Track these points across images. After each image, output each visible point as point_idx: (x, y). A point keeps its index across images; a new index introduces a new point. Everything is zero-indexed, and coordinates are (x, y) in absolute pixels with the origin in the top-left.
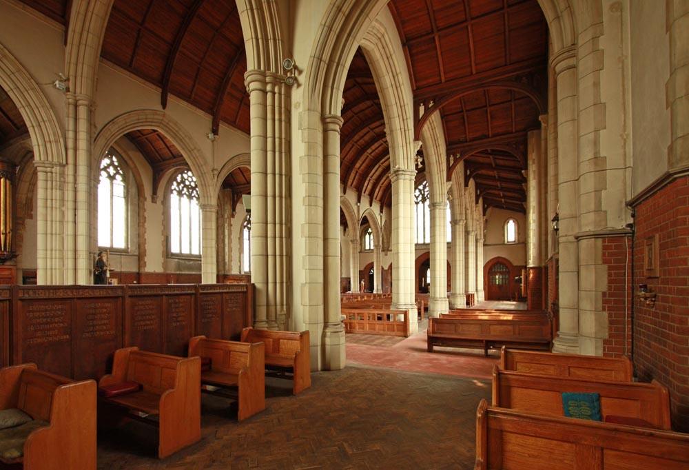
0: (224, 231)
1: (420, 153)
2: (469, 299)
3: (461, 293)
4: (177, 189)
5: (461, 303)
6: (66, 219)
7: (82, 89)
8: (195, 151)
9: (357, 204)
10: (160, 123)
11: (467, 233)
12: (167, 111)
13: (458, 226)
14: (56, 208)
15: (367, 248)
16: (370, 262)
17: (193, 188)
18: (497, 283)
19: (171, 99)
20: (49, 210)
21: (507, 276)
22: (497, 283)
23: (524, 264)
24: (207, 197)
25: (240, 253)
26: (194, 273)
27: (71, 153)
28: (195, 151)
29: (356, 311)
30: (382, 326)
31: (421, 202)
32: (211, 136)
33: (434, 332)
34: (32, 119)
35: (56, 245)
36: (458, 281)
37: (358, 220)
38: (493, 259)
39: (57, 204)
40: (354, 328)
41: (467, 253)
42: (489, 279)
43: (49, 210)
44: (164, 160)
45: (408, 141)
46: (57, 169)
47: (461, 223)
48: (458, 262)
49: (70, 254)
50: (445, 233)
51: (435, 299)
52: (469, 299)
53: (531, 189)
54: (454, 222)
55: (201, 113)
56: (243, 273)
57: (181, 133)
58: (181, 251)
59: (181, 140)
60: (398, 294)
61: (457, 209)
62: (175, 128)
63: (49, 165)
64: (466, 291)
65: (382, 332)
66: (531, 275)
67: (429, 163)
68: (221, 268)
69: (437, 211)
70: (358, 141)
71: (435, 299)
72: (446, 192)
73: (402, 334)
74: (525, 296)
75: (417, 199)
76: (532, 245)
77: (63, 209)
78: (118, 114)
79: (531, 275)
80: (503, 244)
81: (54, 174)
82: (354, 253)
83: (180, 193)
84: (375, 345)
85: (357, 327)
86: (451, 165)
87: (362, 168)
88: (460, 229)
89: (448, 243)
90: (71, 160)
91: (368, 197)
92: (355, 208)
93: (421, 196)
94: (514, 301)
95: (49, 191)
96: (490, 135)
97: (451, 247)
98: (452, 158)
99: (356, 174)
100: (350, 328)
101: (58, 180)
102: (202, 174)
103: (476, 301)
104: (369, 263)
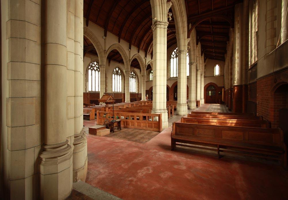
1: (170, 11)
2: (198, 103)
3: (194, 100)
5: (193, 105)
11: (197, 70)
13: (192, 66)
15: (151, 80)
16: (152, 86)
18: (210, 95)
21: (215, 92)
22: (210, 95)
23: (223, 86)
25: (86, 82)
29: (130, 114)
30: (145, 124)
31: (175, 58)
33: (176, 134)
36: (192, 94)
37: (146, 66)
38: (208, 84)
40: (129, 125)
41: (197, 80)
42: (206, 93)
45: (163, 2)
47: (194, 64)
48: (192, 84)
50: (186, 71)
51: (180, 105)
52: (198, 103)
53: (237, 38)
54: (191, 64)
56: (87, 92)
60: (156, 103)
61: (192, 57)
64: (196, 99)
65: (145, 128)
66: (236, 90)
67: (176, 17)
69: (182, 55)
70: (145, 25)
71: (180, 105)
72: (187, 44)
73: (157, 130)
74: (224, 101)
75: (173, 56)
76: (236, 72)
79: (236, 90)
80: (213, 76)
82: (143, 82)
84: (136, 141)
85: (130, 124)
86: (190, 28)
87: (147, 40)
88: (194, 67)
89: (187, 77)
91: (151, 55)
92: (144, 60)
93: (175, 55)
94: (218, 104)
96: (213, 9)
97: (189, 78)
98: (190, 25)
99: (144, 43)
100: (126, 125)
102: (100, 52)
103: (200, 104)
104: (151, 87)
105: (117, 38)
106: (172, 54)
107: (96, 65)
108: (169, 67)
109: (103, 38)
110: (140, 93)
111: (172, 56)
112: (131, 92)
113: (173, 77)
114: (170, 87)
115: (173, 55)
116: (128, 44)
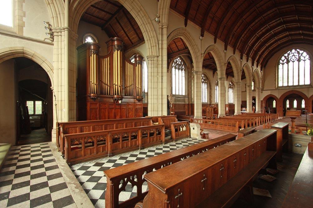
0: (191, 84)
4: (174, 66)
6: (159, 81)
7: (164, 20)
8: (195, 46)
9: (252, 67)
10: (184, 34)
12: (187, 28)
14: (155, 76)
17: (180, 65)
19: (189, 22)
20: (153, 77)
24: (199, 67)
26: (180, 103)
27: (160, 50)
28: (195, 46)
32: (201, 37)
34: (293, 24)
35: (155, 93)
39: (156, 74)
43: (153, 77)
44: (173, 53)
46: (156, 58)
49: (160, 97)
55: (197, 27)
57: (191, 38)
58: (182, 94)
59: (190, 41)
62: (189, 35)
63: (153, 57)
68: (190, 101)
75: (283, 62)
77: (158, 76)
78: (171, 32)
81: (155, 61)
83: (176, 68)
90: (160, 54)
93: (286, 60)
95: (153, 68)
101: (156, 63)
102: (197, 56)
105: (183, 19)
106: (280, 59)
107: (204, 77)
108: (277, 75)
109: (224, 52)
110: (190, 103)
111: (281, 62)
112: (203, 103)
113: (283, 86)
114: (278, 98)
115: (283, 61)
116: (224, 44)
